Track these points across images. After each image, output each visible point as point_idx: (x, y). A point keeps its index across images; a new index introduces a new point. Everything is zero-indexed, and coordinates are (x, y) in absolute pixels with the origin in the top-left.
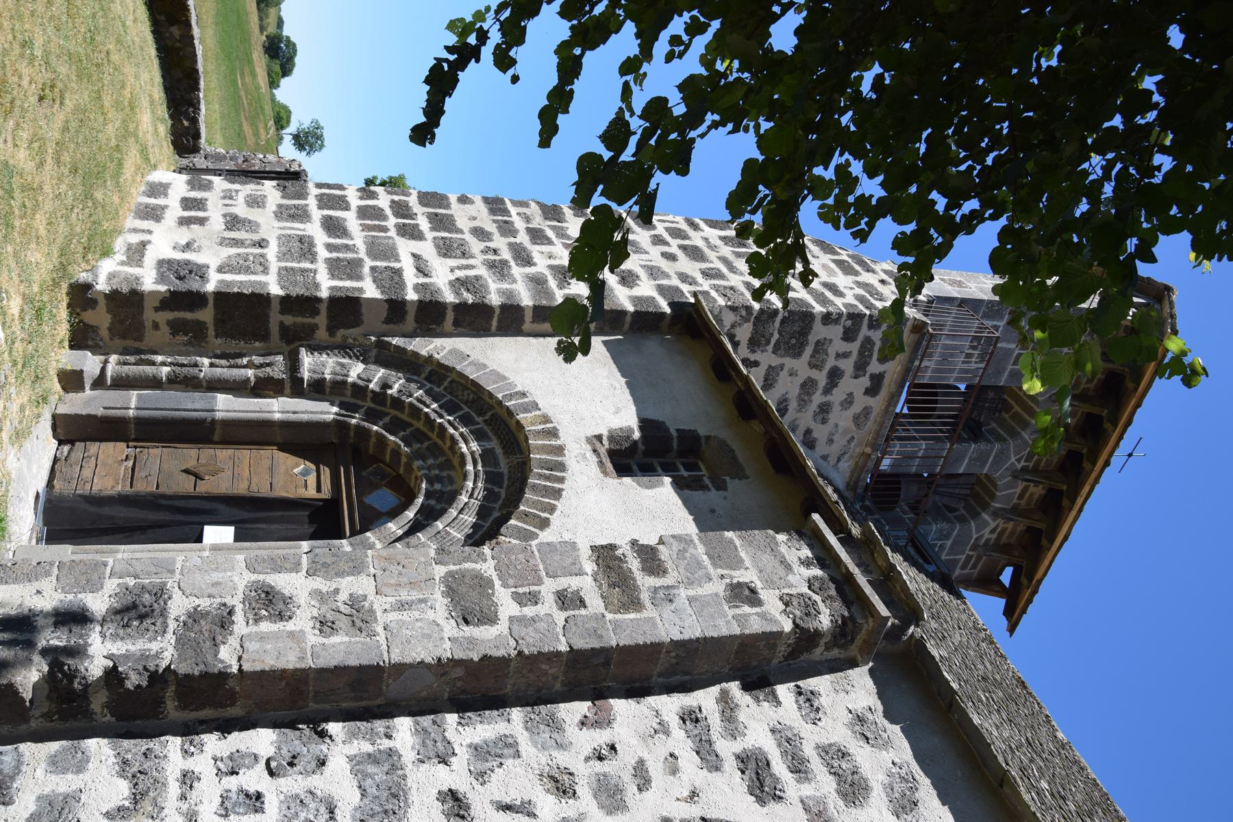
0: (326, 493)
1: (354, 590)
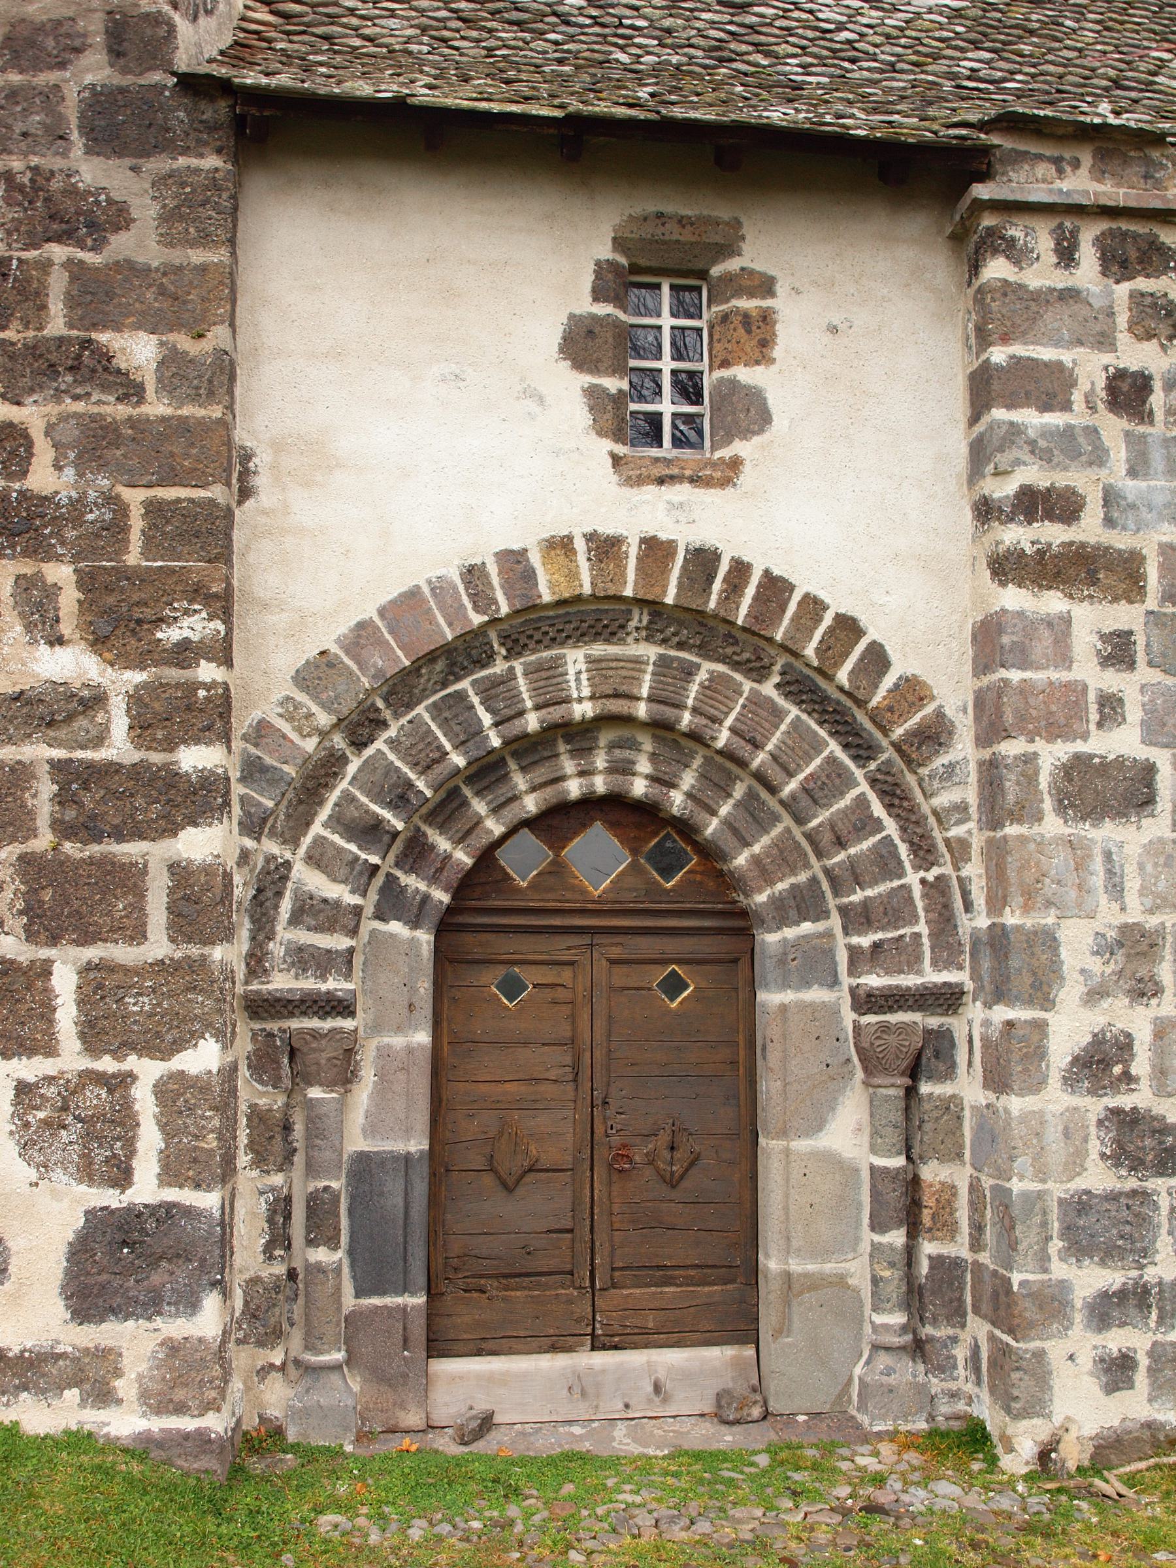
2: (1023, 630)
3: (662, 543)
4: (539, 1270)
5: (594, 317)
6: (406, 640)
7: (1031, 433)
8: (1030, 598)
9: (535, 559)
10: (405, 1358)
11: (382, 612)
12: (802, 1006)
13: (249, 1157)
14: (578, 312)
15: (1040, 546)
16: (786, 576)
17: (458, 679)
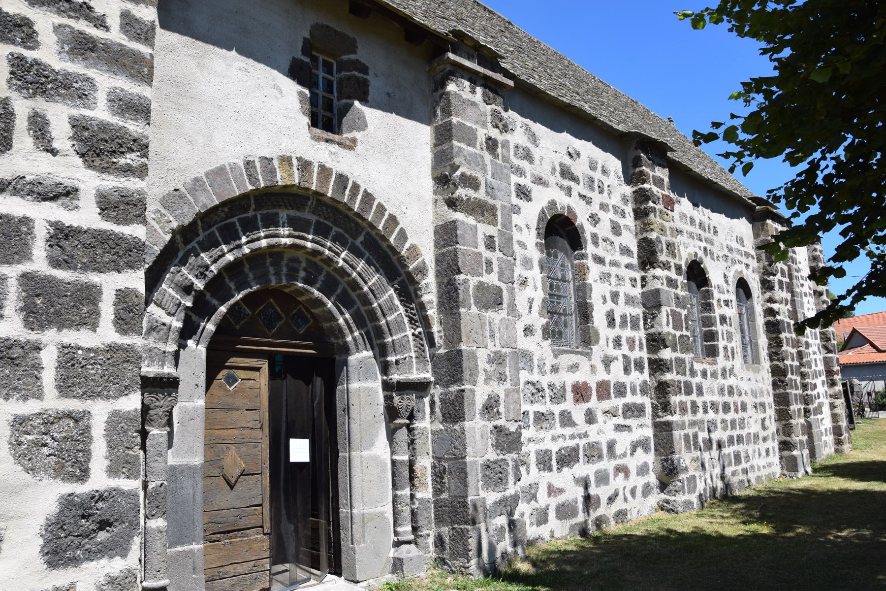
0: (265, 365)
1: (485, 360)
6: (218, 191)
9: (276, 163)
10: (195, 579)
11: (207, 175)
14: (296, 57)
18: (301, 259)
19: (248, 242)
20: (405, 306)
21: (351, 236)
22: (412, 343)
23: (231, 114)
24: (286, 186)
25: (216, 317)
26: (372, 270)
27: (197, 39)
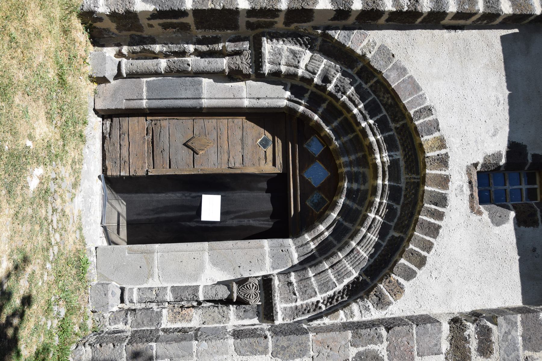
0: (278, 169)
2: (434, 333)
3: (447, 184)
4: (155, 156)
5: (526, 154)
7: (513, 333)
8: (446, 335)
9: (437, 134)
10: (122, 100)
11: (411, 77)
12: (263, 255)
13: (201, 38)
15: (468, 338)
16: (440, 235)
17: (387, 110)
18: (366, 184)
19: (370, 125)
20: (344, 290)
21: (397, 224)
22: (309, 301)
23: (461, 93)
24: (421, 145)
25: (309, 112)
26: (371, 250)
27: (505, 62)
